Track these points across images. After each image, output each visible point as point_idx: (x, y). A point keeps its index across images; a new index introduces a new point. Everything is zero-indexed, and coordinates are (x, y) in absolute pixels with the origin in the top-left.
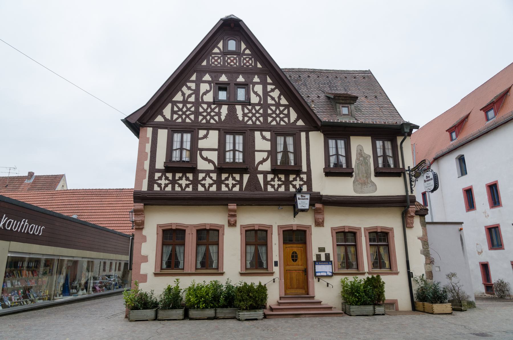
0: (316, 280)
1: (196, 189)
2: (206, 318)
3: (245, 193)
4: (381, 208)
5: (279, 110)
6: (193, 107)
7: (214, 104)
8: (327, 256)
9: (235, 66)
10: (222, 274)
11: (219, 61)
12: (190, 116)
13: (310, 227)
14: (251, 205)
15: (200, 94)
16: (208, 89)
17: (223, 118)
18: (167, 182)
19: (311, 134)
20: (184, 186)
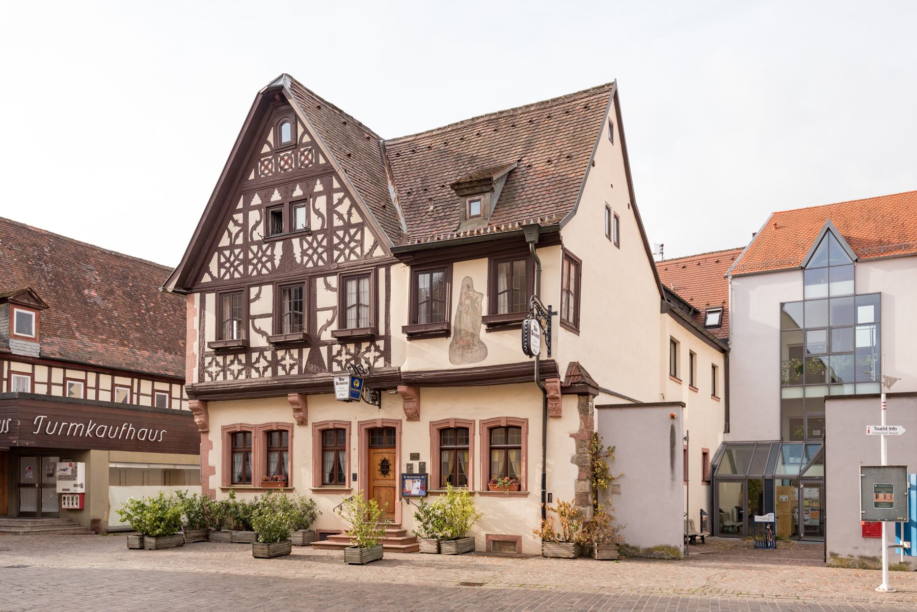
10: (291, 490)
14: (318, 393)
17: (277, 263)
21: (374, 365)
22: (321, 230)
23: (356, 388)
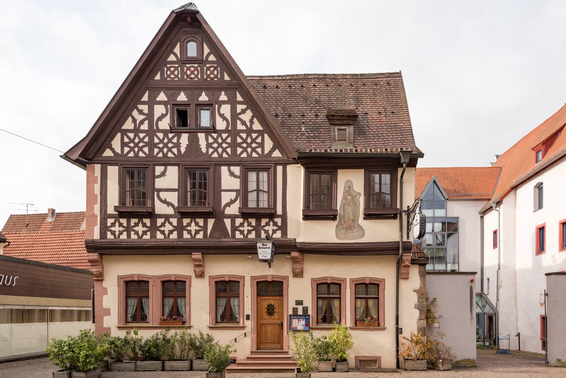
3: (139, 241)
5: (250, 137)
7: (172, 132)
9: (197, 79)
10: (190, 327)
11: (176, 73)
12: (144, 149)
13: (345, 280)
15: (154, 118)
16: (164, 112)
17: (183, 150)
18: (122, 229)
20: (140, 233)
21: (272, 235)
22: (226, 130)
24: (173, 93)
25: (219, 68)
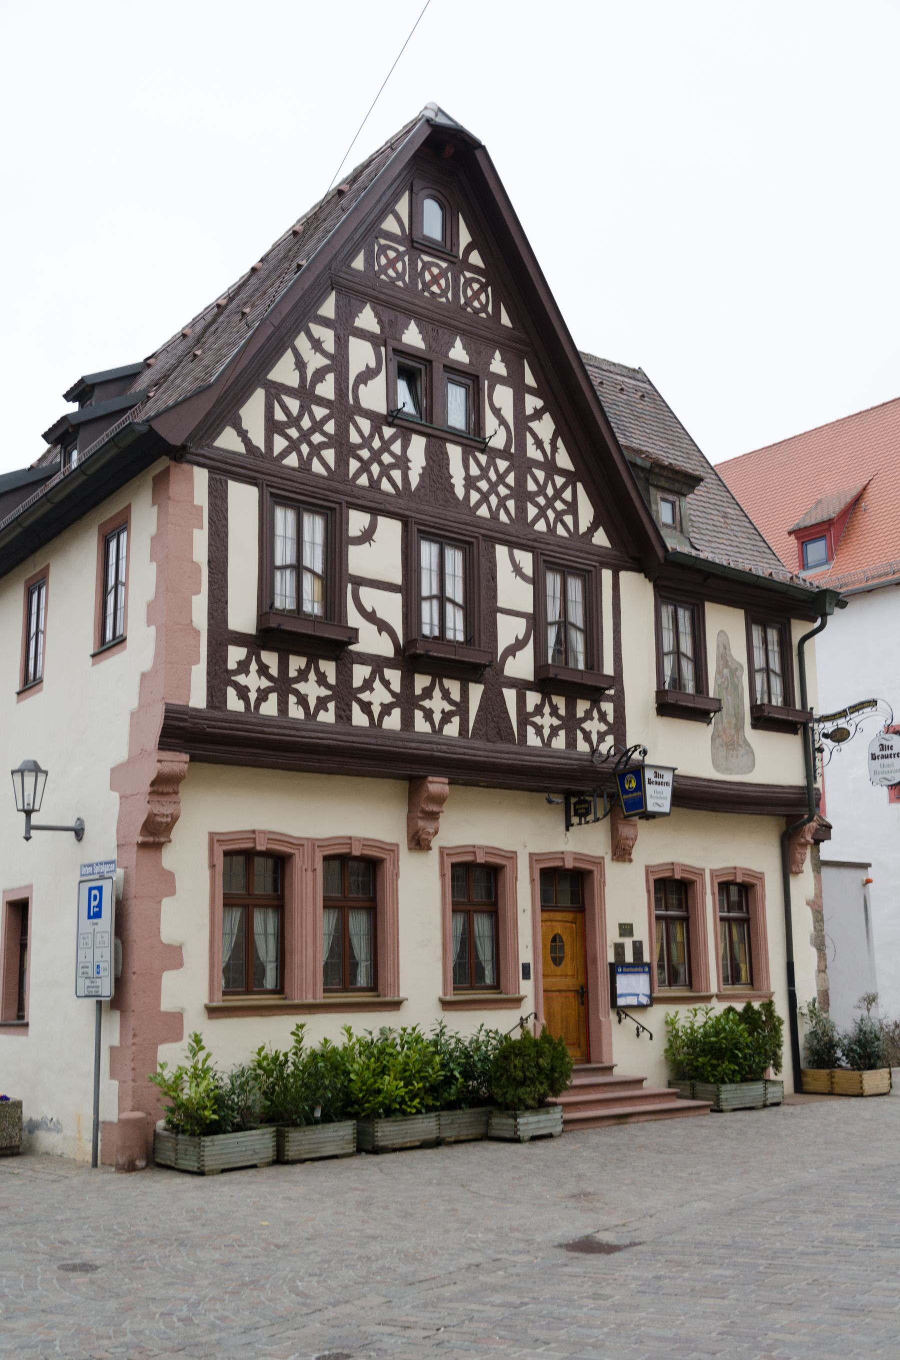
0: (613, 1017)
1: (345, 718)
2: (418, 1144)
4: (742, 816)
6: (330, 419)
7: (390, 425)
8: (638, 948)
10: (396, 1005)
15: (348, 374)
16: (373, 365)
17: (414, 480)
19: (624, 575)
23: (632, 792)
24: (393, 318)
25: (489, 289)
